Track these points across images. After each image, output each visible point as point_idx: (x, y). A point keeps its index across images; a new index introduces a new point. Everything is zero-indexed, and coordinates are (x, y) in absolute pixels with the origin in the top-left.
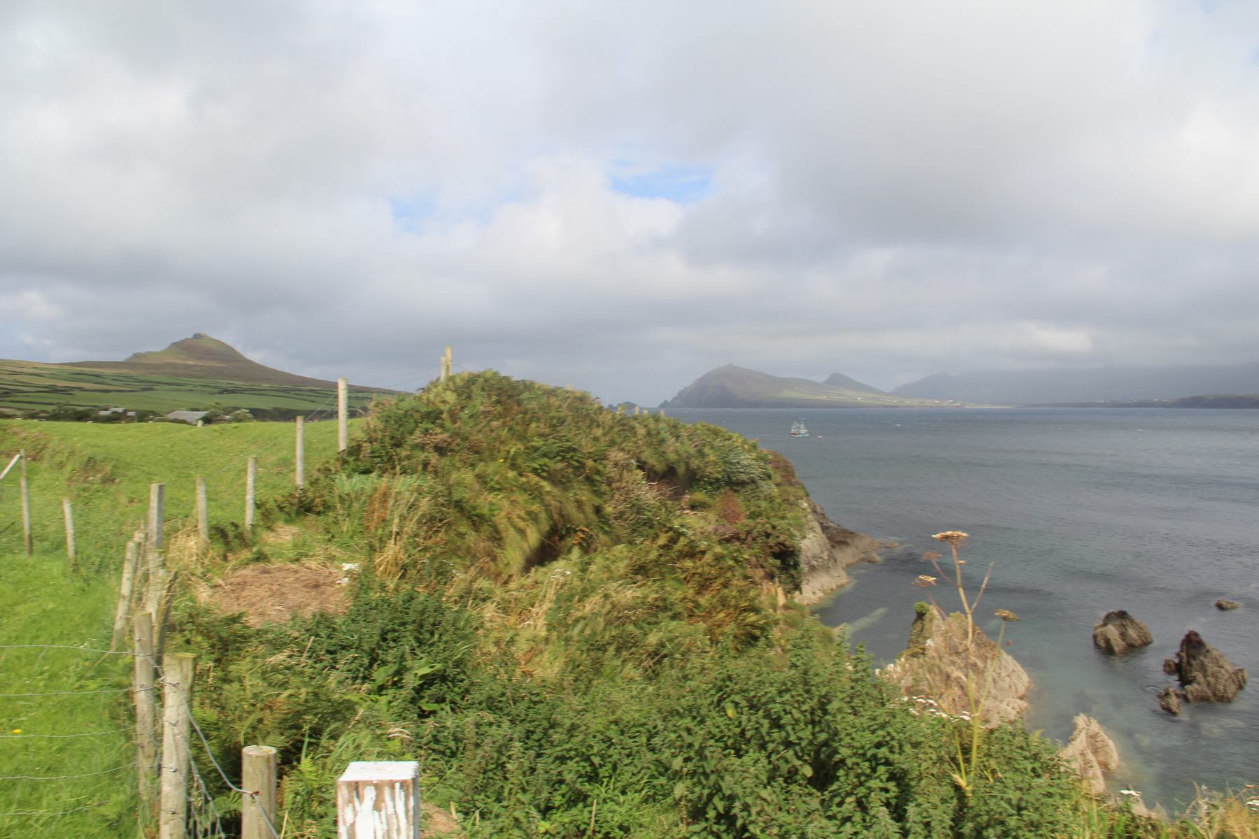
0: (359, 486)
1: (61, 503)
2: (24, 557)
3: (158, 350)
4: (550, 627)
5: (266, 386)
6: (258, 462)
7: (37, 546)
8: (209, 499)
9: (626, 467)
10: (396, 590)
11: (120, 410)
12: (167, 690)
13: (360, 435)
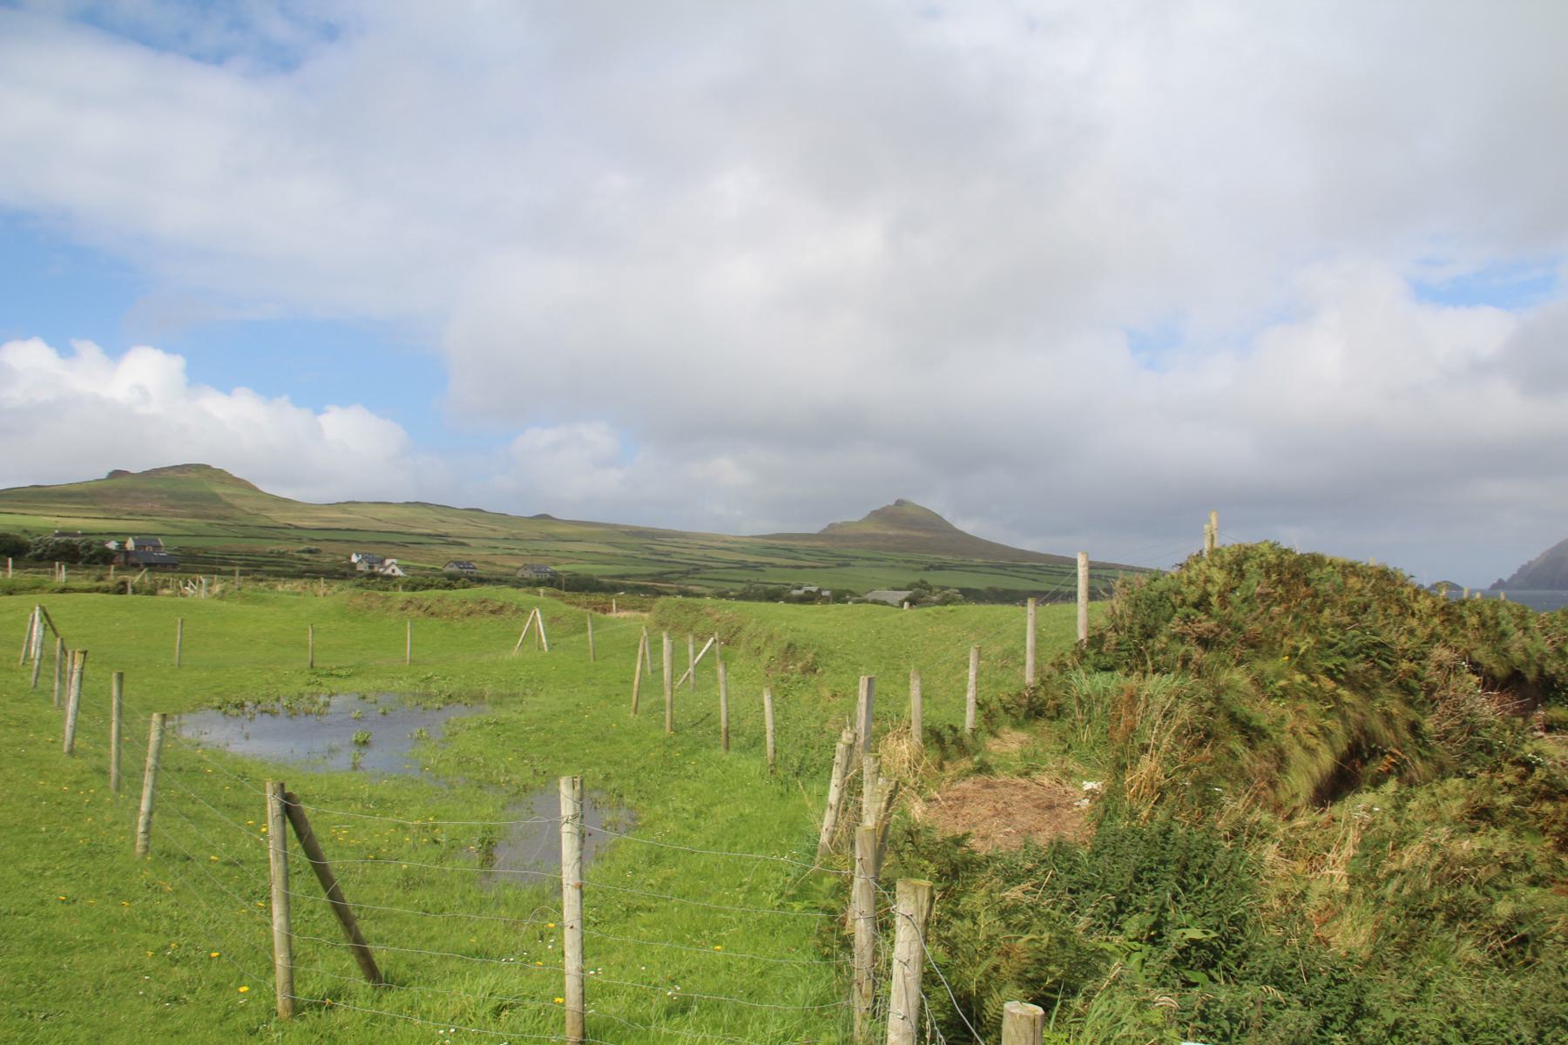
0: (1100, 686)
1: (760, 694)
2: (721, 751)
3: (856, 520)
4: (1353, 880)
5: (979, 561)
6: (978, 655)
7: (734, 741)
8: (923, 696)
9: (1454, 670)
10: (1151, 817)
11: (814, 589)
13: (1103, 622)
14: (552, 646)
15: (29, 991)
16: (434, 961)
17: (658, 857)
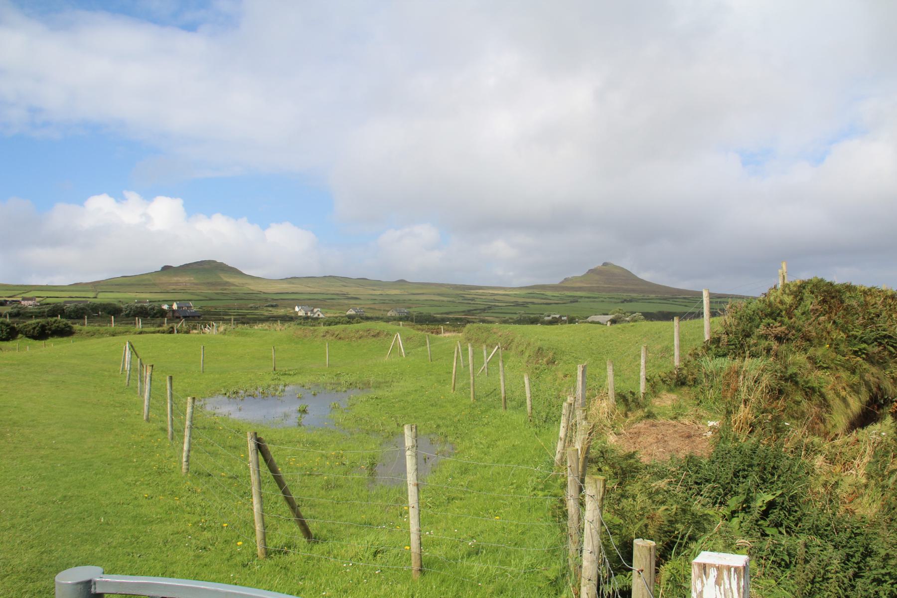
1: (523, 377)
2: (501, 411)
4: (869, 476)
5: (653, 296)
6: (649, 349)
8: (615, 375)
11: (557, 316)
12: (587, 499)
13: (720, 329)
14: (407, 354)
15: (132, 543)
16: (342, 528)
17: (466, 470)
